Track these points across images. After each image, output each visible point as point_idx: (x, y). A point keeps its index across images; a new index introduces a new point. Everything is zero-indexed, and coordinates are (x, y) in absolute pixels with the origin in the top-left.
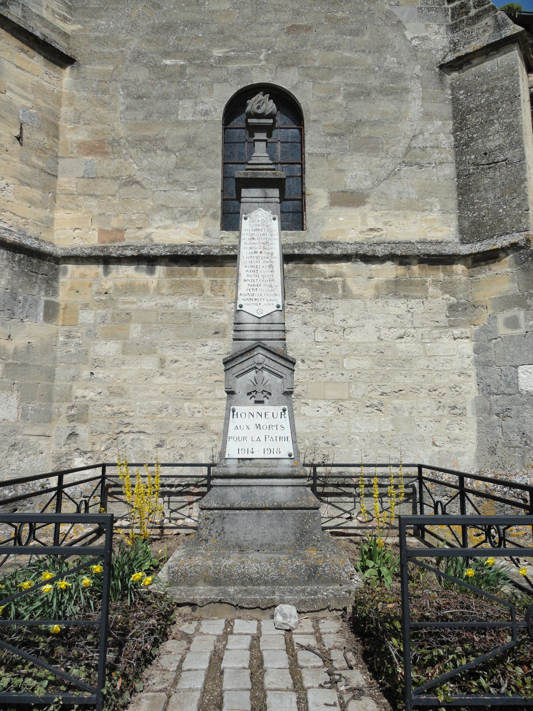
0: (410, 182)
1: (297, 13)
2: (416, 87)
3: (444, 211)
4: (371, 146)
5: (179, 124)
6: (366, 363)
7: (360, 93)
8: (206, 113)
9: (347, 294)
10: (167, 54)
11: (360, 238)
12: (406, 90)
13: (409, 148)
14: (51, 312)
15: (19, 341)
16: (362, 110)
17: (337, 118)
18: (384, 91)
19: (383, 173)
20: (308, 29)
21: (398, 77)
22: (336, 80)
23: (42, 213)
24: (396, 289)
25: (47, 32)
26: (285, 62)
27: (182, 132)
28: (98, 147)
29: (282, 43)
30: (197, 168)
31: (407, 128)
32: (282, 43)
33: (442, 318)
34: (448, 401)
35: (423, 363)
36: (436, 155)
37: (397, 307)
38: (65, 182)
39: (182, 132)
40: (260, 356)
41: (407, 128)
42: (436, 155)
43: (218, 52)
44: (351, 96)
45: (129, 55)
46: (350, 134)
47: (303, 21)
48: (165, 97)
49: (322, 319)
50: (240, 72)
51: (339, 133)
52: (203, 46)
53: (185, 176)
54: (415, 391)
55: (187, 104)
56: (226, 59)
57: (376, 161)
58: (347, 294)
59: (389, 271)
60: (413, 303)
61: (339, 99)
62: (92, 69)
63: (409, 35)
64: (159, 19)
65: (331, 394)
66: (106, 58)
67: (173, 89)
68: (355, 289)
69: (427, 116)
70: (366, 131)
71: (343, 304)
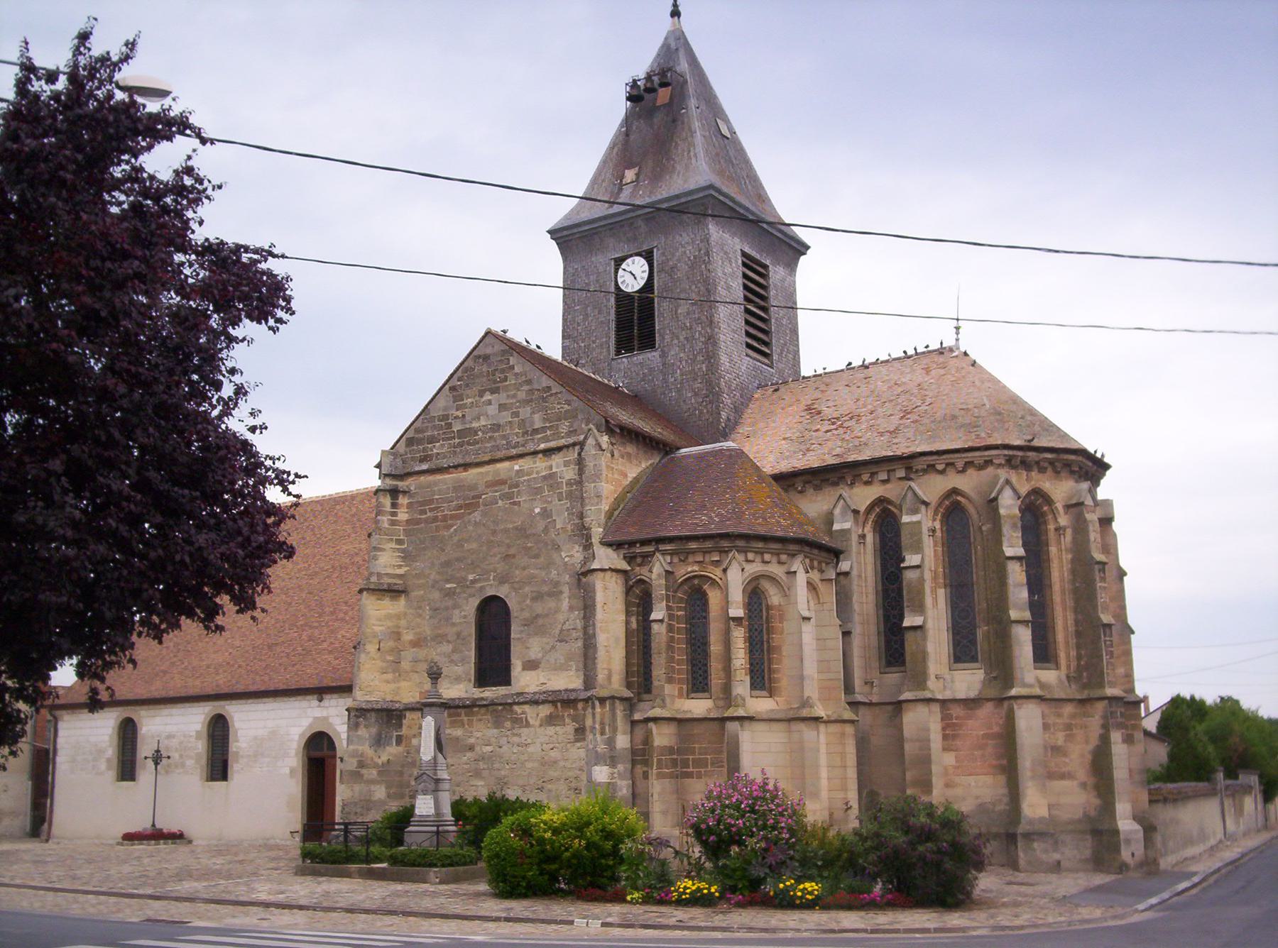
0: (559, 656)
1: (509, 546)
2: (566, 589)
3: (577, 670)
4: (541, 631)
5: (454, 624)
6: (536, 765)
7: (538, 597)
8: (465, 617)
9: (528, 725)
10: (448, 581)
11: (537, 689)
12: (561, 592)
13: (562, 630)
14: (399, 740)
15: (384, 758)
16: (539, 608)
17: (526, 614)
18: (550, 594)
19: (548, 647)
20: (514, 556)
21: (557, 584)
22: (527, 589)
23: (393, 686)
24: (551, 720)
25: (390, 581)
26: (503, 580)
27: (455, 629)
28: (416, 644)
29: (501, 567)
30: (461, 652)
31: (561, 617)
32: (501, 567)
33: (571, 737)
34: (573, 785)
35: (562, 763)
36: (574, 635)
37: (551, 730)
38: (405, 665)
39: (455, 629)
40: (425, 777)
41: (561, 617)
42: (574, 635)
43: (471, 577)
44: (534, 599)
45: (430, 582)
46: (535, 624)
47: (512, 551)
48: (447, 608)
49: (516, 739)
50: (482, 588)
51: (527, 623)
52: (464, 574)
53: (456, 657)
54: (558, 779)
55: (456, 612)
56: (474, 582)
57: (545, 640)
58: (528, 725)
59: (545, 710)
60: (558, 728)
61: (528, 602)
62: (416, 594)
63: (563, 555)
64: (443, 559)
65: (521, 782)
66: (420, 587)
67: (450, 603)
68: (531, 722)
69: (571, 608)
70: (540, 621)
71: (525, 730)
